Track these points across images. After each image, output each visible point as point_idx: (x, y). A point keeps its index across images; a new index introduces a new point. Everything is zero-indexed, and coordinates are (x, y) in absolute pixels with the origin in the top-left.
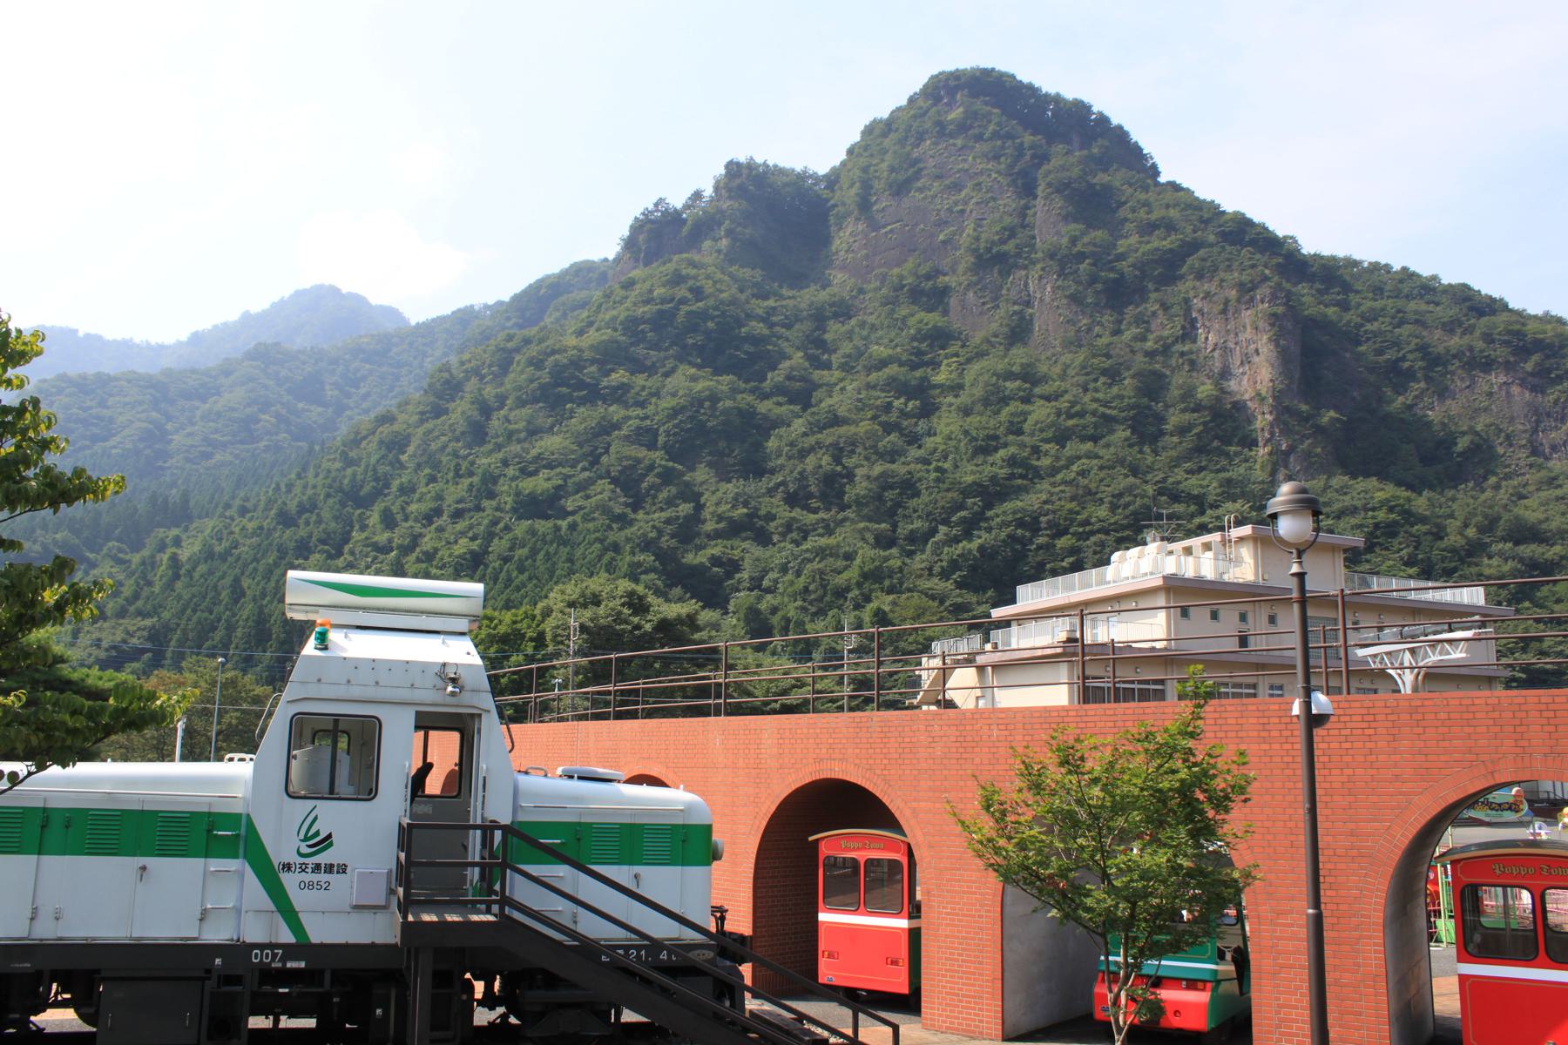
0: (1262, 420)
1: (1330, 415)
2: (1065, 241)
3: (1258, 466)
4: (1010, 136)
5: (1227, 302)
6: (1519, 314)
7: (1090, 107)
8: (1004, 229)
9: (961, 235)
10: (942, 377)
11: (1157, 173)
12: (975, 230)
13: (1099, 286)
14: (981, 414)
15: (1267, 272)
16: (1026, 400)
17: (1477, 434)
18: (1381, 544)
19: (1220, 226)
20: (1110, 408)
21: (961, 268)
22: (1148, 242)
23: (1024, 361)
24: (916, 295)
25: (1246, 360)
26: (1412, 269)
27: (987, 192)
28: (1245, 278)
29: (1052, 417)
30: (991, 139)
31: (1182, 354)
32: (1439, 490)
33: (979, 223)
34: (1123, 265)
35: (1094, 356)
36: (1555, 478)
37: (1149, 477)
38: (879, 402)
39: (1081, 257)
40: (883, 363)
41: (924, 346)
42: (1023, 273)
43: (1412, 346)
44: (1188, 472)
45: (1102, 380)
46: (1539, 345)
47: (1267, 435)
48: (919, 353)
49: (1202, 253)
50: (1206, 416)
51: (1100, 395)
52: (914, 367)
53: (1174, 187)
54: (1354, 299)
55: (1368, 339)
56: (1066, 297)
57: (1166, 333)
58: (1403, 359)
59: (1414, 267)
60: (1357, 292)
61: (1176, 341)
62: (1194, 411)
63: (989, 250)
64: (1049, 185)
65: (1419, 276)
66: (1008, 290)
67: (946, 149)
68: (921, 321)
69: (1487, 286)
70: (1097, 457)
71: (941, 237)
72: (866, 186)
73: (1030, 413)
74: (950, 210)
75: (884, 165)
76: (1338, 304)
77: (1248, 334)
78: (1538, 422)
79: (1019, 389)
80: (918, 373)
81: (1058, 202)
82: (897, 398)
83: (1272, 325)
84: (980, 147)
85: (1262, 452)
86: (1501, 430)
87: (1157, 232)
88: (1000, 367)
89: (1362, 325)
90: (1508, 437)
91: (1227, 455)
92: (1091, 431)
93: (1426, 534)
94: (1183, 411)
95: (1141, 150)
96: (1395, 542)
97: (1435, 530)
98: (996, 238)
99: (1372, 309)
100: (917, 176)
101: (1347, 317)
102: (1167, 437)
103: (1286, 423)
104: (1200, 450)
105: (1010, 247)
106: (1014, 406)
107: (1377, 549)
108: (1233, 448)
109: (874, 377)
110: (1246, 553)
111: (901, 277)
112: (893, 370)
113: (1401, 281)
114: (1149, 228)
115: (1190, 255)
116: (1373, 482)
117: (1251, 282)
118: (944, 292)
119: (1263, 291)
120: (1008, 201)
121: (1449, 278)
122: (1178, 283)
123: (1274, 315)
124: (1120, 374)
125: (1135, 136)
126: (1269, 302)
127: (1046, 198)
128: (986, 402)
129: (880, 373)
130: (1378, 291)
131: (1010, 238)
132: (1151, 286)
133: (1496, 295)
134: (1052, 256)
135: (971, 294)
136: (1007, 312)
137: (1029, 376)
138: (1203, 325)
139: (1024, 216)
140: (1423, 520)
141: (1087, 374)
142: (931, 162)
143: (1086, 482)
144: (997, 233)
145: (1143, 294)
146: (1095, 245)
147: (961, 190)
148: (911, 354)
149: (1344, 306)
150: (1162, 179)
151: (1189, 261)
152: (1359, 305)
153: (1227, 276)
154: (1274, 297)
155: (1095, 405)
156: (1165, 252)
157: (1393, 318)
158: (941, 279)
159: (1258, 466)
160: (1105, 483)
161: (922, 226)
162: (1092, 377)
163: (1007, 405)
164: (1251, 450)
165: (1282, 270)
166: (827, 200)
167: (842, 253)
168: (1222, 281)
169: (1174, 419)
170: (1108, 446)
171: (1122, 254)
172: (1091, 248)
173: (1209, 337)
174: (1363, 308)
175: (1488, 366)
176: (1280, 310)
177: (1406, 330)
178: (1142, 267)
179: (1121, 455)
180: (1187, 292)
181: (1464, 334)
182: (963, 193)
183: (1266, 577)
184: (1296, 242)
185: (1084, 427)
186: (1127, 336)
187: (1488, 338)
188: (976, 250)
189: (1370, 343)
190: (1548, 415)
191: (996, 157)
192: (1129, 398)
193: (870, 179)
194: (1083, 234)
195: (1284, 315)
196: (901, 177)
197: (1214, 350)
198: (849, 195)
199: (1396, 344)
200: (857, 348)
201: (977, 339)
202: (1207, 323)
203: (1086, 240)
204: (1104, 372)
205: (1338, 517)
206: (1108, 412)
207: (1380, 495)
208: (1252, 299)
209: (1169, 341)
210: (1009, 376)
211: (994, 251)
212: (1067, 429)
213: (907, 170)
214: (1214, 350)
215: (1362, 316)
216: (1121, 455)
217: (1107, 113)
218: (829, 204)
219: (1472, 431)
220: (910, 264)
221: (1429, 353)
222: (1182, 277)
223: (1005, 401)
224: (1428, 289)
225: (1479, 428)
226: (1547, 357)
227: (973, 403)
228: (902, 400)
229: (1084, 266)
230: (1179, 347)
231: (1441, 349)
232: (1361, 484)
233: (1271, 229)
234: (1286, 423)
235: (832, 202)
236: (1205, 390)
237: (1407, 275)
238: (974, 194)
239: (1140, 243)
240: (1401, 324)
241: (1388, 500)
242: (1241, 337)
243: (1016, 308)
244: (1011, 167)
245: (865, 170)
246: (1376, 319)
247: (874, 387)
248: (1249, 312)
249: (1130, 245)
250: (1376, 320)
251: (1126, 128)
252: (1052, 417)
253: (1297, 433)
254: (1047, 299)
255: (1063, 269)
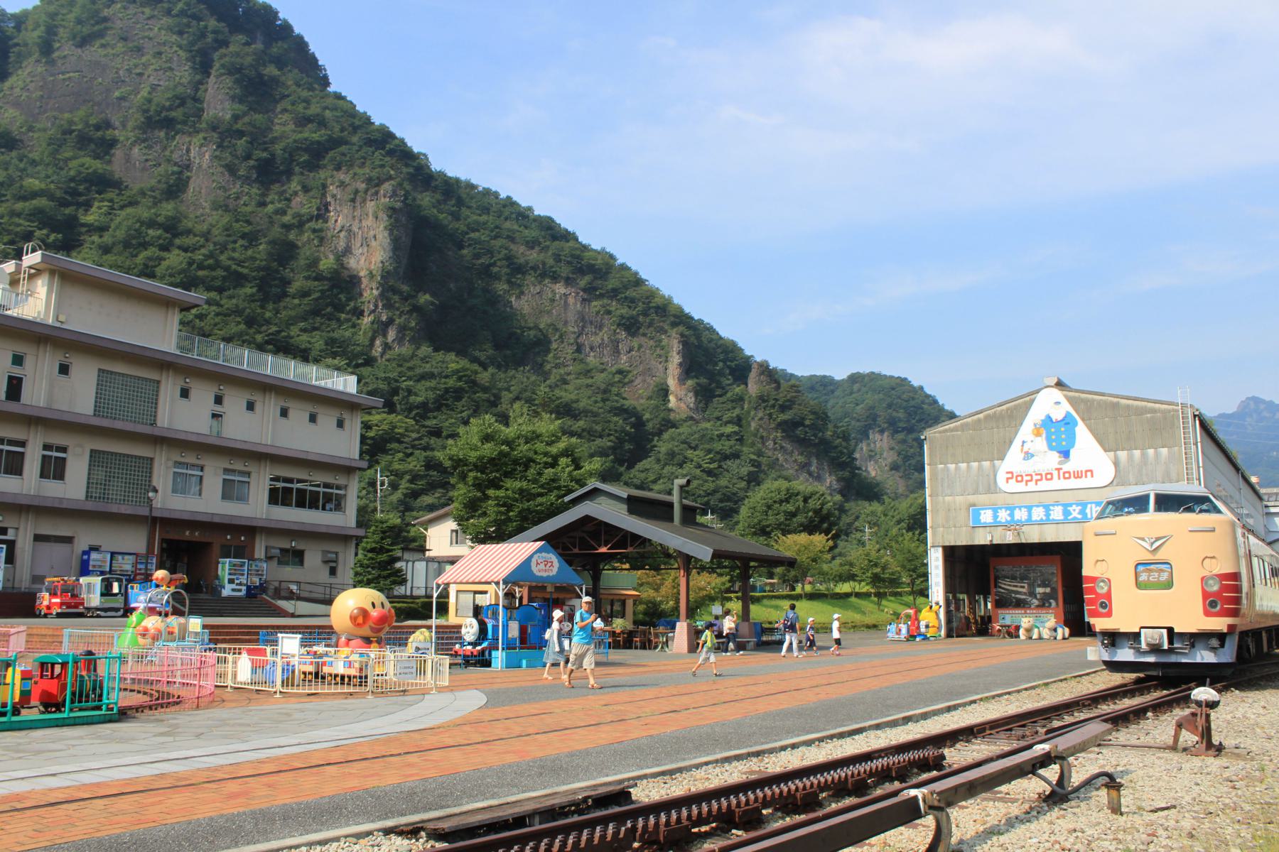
0: (370, 292)
1: (424, 298)
2: (228, 117)
3: (361, 333)
4: (194, 17)
5: (357, 192)
6: (585, 248)
7: (277, 13)
8: (177, 97)
9: (136, 95)
10: (91, 217)
11: (328, 84)
12: (149, 93)
13: (252, 163)
14: (120, 254)
15: (392, 172)
16: (165, 248)
17: (541, 330)
18: (447, 405)
19: (367, 133)
20: (243, 267)
21: (130, 124)
22: (301, 132)
23: (169, 214)
24: (83, 141)
25: (366, 243)
26: (515, 199)
27: (166, 62)
28: (374, 174)
29: (184, 265)
30: (177, 16)
31: (314, 231)
32: (503, 369)
33: (154, 88)
34: (278, 148)
35: (237, 221)
36: (589, 371)
37: (264, 328)
38: (18, 229)
39: (241, 134)
40: (34, 195)
41: (81, 188)
42: (187, 139)
43: (501, 256)
44: (301, 330)
45: (241, 242)
46: (591, 269)
47: (372, 307)
48: (75, 193)
49: (343, 148)
50: (325, 285)
51: (236, 255)
52: (63, 203)
53: (339, 97)
54: (465, 212)
55: (470, 245)
56: (221, 166)
57: (304, 211)
58: (494, 264)
59: (516, 198)
60: (469, 207)
61: (310, 220)
62: (316, 279)
63: (159, 113)
64: (223, 66)
65: (518, 205)
66: (172, 152)
67: (135, 14)
68: (83, 165)
69: (565, 221)
70: (218, 305)
71: (117, 94)
72: (51, 31)
73: (165, 259)
74: (129, 71)
75: (71, 17)
76: (452, 214)
77: (369, 221)
78: (583, 327)
79: (159, 238)
80: (67, 211)
81: (228, 81)
82: (40, 229)
83: (390, 217)
84: (166, 21)
85: (367, 320)
86: (557, 330)
87: (310, 126)
88: (146, 215)
89: (467, 233)
90: (561, 337)
91: (338, 320)
92: (218, 283)
93: (484, 400)
94: (307, 278)
95: (316, 60)
96: (459, 404)
97: (492, 399)
98: (167, 104)
99: (477, 223)
100: (101, 34)
101: (455, 225)
102: (288, 299)
103: (388, 299)
104: (316, 312)
105: (177, 114)
106: (152, 252)
107: (444, 409)
108: (343, 316)
109: (19, 206)
110: (42, 287)
111: (71, 122)
112: (42, 202)
113: (504, 206)
114: (303, 121)
115: (332, 149)
116: (452, 356)
117: (378, 178)
118: (113, 143)
119: (387, 187)
120: (184, 74)
121: (539, 211)
122: (321, 172)
123: (393, 209)
124: (257, 239)
125: (313, 48)
126: (390, 197)
127: (217, 77)
128: (127, 244)
129: (27, 204)
130: (486, 210)
131: (178, 106)
132: (297, 169)
133: (570, 229)
134: (214, 128)
135: (136, 150)
136: (167, 171)
137: (172, 228)
138: (335, 209)
139: (197, 90)
140: (485, 390)
141: (229, 236)
142: (119, 24)
143: (203, 324)
144: (168, 99)
145: (289, 173)
146: (254, 126)
147: (143, 55)
148: (66, 193)
149: (456, 217)
150: (331, 89)
151: (331, 154)
152: (469, 217)
153: (360, 171)
154: (394, 194)
155: (230, 263)
156: (312, 143)
157: (492, 231)
158: (109, 132)
159: (361, 333)
160: (219, 326)
161: (100, 80)
162: (231, 239)
163: (146, 249)
164: (359, 319)
165: (412, 178)
166: (11, 38)
167: (18, 90)
168: (355, 174)
169: (298, 284)
170: (231, 297)
171: (276, 138)
172: (250, 128)
173: (339, 218)
174: (469, 220)
175: (555, 278)
176: (398, 205)
177: (497, 243)
178: (291, 153)
179: (241, 307)
180: (326, 179)
181: (541, 251)
182: (144, 59)
183: (62, 318)
184: (427, 159)
185: (214, 278)
186: (270, 208)
187: (557, 258)
188: (147, 111)
189: (471, 248)
190: (591, 323)
191: (181, 33)
192: (261, 261)
193: (56, 27)
194: (245, 114)
195: (401, 209)
196: (86, 30)
197: (341, 231)
198: (32, 36)
199: (490, 252)
200: (10, 177)
201: (136, 187)
202: (338, 208)
203: (246, 119)
204: (244, 236)
205: (418, 381)
206: (240, 269)
207: (453, 366)
208: (377, 193)
209: (305, 218)
210: (152, 224)
211: (163, 115)
212: (197, 278)
213: (93, 25)
214: (341, 231)
215: (468, 226)
216: (241, 307)
217: (291, 22)
218: (11, 43)
219: (536, 327)
220: (81, 113)
221: (515, 264)
222: (325, 166)
223: (145, 245)
224: (523, 215)
225: (542, 326)
226: (595, 278)
227: (114, 244)
228: (45, 232)
229: (241, 143)
230: (312, 225)
231: (522, 261)
232: (440, 356)
233: (409, 145)
234: (388, 299)
235: (15, 41)
236: (327, 263)
237: (510, 203)
238: (154, 61)
239: (294, 131)
240: (496, 237)
241: (458, 371)
242: (364, 223)
243: (175, 169)
244: (192, 44)
245: (53, 16)
246: (478, 230)
247: (19, 215)
248: (373, 203)
249: (284, 132)
250: (478, 231)
251: (306, 39)
252: (184, 265)
253: (398, 309)
254: (205, 166)
255: (223, 140)
